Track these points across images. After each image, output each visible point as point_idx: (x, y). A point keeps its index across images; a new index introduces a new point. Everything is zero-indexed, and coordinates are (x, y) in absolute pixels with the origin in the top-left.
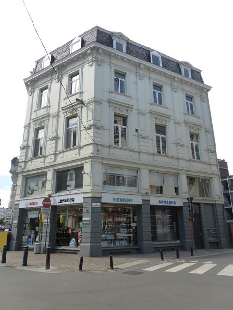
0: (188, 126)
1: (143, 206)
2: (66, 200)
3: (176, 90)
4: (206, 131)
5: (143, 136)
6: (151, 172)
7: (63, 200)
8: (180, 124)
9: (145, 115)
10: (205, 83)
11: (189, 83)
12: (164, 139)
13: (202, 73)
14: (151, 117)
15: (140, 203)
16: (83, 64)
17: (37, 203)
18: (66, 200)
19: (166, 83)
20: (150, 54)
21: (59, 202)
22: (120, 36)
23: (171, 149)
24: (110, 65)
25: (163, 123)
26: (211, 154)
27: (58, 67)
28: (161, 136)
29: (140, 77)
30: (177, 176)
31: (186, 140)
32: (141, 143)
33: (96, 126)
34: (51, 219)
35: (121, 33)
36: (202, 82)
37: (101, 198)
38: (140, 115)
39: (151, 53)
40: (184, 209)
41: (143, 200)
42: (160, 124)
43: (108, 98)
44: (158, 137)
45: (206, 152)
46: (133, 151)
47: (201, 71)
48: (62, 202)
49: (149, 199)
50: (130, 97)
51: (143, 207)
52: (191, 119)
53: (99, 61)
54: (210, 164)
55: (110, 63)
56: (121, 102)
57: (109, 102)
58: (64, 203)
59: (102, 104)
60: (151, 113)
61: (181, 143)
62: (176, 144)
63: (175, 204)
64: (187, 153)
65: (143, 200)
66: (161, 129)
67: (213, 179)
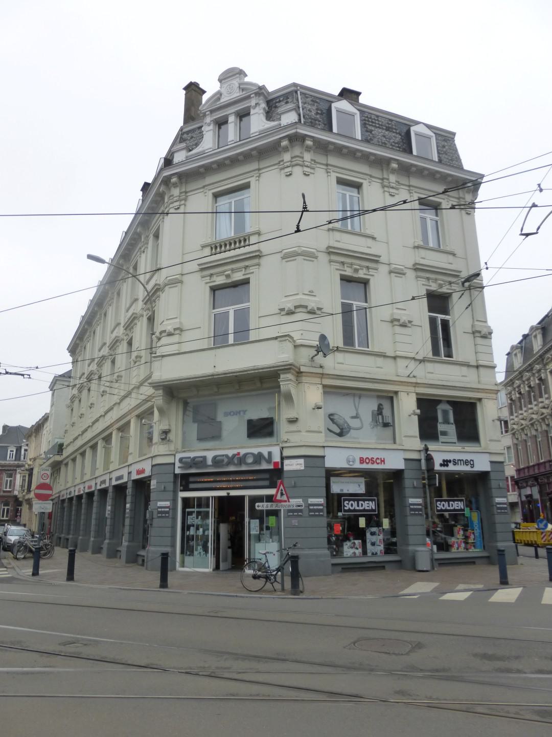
1: (491, 472)
2: (455, 463)
5: (309, 308)
6: (328, 390)
7: (450, 461)
12: (445, 324)
13: (458, 141)
14: (330, 261)
15: (487, 468)
16: (259, 169)
18: (455, 463)
19: (371, 176)
20: (408, 133)
21: (441, 465)
23: (382, 337)
24: (326, 169)
26: (398, 329)
27: (180, 176)
28: (440, 317)
29: (391, 190)
30: (391, 397)
32: (399, 338)
34: (132, 503)
36: (460, 167)
37: (324, 457)
38: (393, 275)
39: (412, 129)
41: (405, 459)
42: (352, 277)
43: (413, 263)
44: (433, 321)
45: (390, 325)
46: (468, 365)
47: (454, 134)
48: (447, 465)
50: (374, 238)
51: (492, 476)
53: (306, 163)
54: (477, 367)
57: (418, 268)
58: (451, 467)
59: (404, 274)
60: (416, 270)
61: (404, 319)
62: (392, 322)
63: (473, 466)
65: (405, 459)
66: (355, 283)
67: (485, 401)
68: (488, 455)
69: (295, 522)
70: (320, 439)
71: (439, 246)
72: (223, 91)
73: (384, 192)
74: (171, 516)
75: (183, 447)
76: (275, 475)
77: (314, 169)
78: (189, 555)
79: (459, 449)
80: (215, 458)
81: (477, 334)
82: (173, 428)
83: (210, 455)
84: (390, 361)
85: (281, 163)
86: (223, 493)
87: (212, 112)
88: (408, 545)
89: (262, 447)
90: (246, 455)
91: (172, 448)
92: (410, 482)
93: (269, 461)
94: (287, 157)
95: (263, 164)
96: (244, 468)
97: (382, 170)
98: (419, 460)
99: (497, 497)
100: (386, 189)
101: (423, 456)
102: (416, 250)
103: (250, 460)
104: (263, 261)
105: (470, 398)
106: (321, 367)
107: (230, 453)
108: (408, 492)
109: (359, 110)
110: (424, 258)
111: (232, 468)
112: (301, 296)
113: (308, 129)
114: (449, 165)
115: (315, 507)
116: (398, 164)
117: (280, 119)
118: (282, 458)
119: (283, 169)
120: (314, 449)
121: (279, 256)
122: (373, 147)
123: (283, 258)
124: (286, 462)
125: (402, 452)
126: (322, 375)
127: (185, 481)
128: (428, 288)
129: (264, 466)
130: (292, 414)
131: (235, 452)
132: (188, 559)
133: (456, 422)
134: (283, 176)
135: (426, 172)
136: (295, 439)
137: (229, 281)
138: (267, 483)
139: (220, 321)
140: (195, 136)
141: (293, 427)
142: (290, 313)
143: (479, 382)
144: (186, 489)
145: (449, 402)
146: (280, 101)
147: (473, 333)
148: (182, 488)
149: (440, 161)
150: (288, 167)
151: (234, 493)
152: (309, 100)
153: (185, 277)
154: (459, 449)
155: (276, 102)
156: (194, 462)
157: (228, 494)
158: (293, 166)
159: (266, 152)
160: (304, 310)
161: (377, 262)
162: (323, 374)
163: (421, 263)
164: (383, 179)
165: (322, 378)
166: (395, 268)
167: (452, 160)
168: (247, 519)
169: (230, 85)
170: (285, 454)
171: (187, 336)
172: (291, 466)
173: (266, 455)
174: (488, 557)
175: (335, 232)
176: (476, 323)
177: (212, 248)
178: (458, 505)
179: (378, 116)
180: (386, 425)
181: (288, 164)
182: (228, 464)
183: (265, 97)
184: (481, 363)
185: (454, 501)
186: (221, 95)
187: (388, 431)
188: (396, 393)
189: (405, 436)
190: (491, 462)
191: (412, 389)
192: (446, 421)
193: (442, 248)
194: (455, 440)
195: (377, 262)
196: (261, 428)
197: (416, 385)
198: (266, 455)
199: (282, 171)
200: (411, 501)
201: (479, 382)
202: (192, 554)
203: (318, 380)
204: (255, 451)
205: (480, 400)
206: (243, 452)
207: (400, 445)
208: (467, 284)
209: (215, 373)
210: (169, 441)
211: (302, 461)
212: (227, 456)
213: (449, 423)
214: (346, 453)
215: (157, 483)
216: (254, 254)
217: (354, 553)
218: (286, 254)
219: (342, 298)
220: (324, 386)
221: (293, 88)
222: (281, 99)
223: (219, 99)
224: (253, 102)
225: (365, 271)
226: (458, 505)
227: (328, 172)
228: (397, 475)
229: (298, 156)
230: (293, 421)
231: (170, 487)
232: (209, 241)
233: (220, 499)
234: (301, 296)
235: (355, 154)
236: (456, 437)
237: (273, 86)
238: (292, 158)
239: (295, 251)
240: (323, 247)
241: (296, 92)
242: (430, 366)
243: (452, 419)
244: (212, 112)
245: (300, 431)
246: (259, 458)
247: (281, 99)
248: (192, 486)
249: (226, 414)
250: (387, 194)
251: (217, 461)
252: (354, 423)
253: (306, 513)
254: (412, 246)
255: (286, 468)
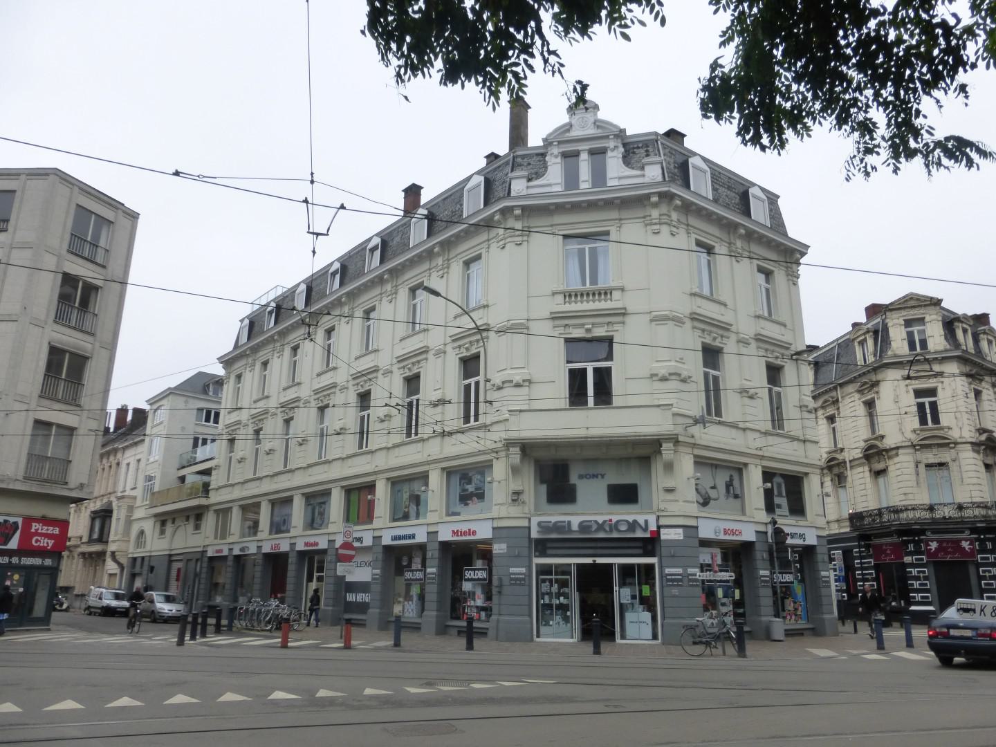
0: (761, 348)
3: (674, 229)
4: (739, 341)
6: (700, 462)
8: (684, 323)
9: (749, 344)
10: (790, 235)
11: (714, 217)
13: (780, 202)
16: (620, 219)
17: (413, 537)
19: (722, 240)
22: (911, 298)
23: (733, 407)
24: (687, 230)
25: (717, 343)
26: (747, 401)
28: (712, 372)
30: (739, 469)
31: (759, 378)
33: (748, 392)
35: (912, 294)
36: (785, 234)
38: (741, 344)
40: (819, 550)
42: (710, 344)
44: (706, 375)
49: (695, 524)
52: (772, 331)
53: (674, 223)
54: (804, 441)
55: (688, 225)
56: (705, 316)
60: (693, 319)
61: (685, 374)
64: (760, 412)
68: (814, 529)
69: (675, 591)
70: (694, 509)
71: (712, 294)
72: (573, 122)
73: (788, 280)
74: (527, 583)
75: (535, 510)
76: (650, 544)
77: (678, 228)
78: (545, 625)
79: (793, 522)
80: (581, 524)
81: (804, 409)
82: (526, 490)
83: (575, 521)
84: (741, 432)
85: (648, 218)
86: (589, 561)
87: (560, 143)
88: (823, 613)
89: (623, 514)
90: (618, 522)
91: (526, 510)
92: (761, 554)
93: (645, 529)
94: (655, 213)
95: (625, 214)
96: (615, 535)
97: (729, 233)
98: (766, 533)
99: (512, 567)
100: (790, 278)
101: (770, 530)
102: (693, 297)
103: (623, 527)
104: (628, 319)
105: (799, 472)
106: (693, 437)
107: (600, 519)
108: (759, 564)
109: (710, 168)
110: (699, 307)
111: (601, 535)
112: (673, 363)
113: (682, 189)
114: (777, 232)
115: (673, 577)
116: (745, 230)
117: (642, 168)
118: (659, 527)
119: (651, 224)
120: (681, 518)
121: (648, 317)
122: (719, 207)
123: (651, 321)
124: (663, 531)
125: (753, 524)
126: (694, 445)
127: (542, 547)
128: (704, 340)
129: (639, 534)
130: (670, 484)
131: (607, 518)
132: (543, 629)
133: (787, 495)
134: (649, 232)
135: (704, 212)
136: (674, 508)
137: (589, 336)
138: (640, 551)
139: (577, 378)
140: (532, 163)
141: (669, 497)
142: (664, 379)
143: (806, 457)
144: (543, 554)
145: (783, 476)
146: (638, 148)
147: (801, 407)
148: (537, 554)
149: (716, 201)
150: (656, 224)
151: (600, 560)
152: (667, 151)
153: (530, 323)
154: (793, 522)
155: (634, 148)
156: (557, 527)
157: (595, 561)
158: (660, 224)
159: (630, 203)
160: (677, 378)
161: (728, 330)
162: (695, 444)
163: (698, 312)
164: (730, 244)
165: (693, 448)
166: (743, 338)
167: (779, 226)
168: (616, 588)
169: (583, 118)
170: (661, 524)
171: (538, 391)
172: (666, 535)
173: (643, 524)
174: (813, 629)
175: (697, 298)
176: (803, 397)
177: (565, 296)
178: (788, 578)
179: (720, 173)
180: (736, 496)
181: (657, 221)
182: (597, 531)
183: (622, 140)
184: (808, 437)
185: (786, 573)
186: (571, 126)
187: (738, 502)
188: (746, 465)
189: (756, 509)
190: (757, 532)
191: (758, 462)
192: (780, 495)
193: (773, 317)
194: (788, 514)
195: (728, 330)
196: (624, 495)
197: (762, 457)
198: (643, 524)
199: (649, 227)
200: (762, 572)
201: (806, 457)
202: (547, 624)
203: (690, 450)
204: (630, 518)
205: (807, 474)
206: (615, 518)
207: (750, 517)
208: (794, 357)
209: (590, 436)
210: (523, 502)
211: (680, 531)
212: (596, 522)
213: (782, 496)
214: (714, 524)
215: (698, 557)
216: (619, 312)
217: (712, 623)
218: (656, 316)
219: (704, 367)
220: (695, 456)
221: (653, 137)
222: (640, 145)
223: (568, 131)
224: (611, 144)
225: (719, 339)
226: (788, 578)
227: (688, 233)
228: (748, 546)
229: (665, 215)
230: (669, 490)
231: (525, 552)
232: (561, 288)
233: (579, 566)
234: (673, 363)
235: (711, 216)
236: (787, 511)
237: (634, 127)
238: (660, 215)
239: (666, 316)
240: (687, 312)
241: (657, 141)
242: (771, 440)
243: (784, 494)
244: (560, 143)
245: (677, 501)
246: (633, 526)
247: (640, 145)
248: (549, 552)
249: (581, 477)
250: (791, 282)
251: (584, 527)
252: (713, 494)
253: (686, 582)
254: (753, 315)
255: (663, 537)
